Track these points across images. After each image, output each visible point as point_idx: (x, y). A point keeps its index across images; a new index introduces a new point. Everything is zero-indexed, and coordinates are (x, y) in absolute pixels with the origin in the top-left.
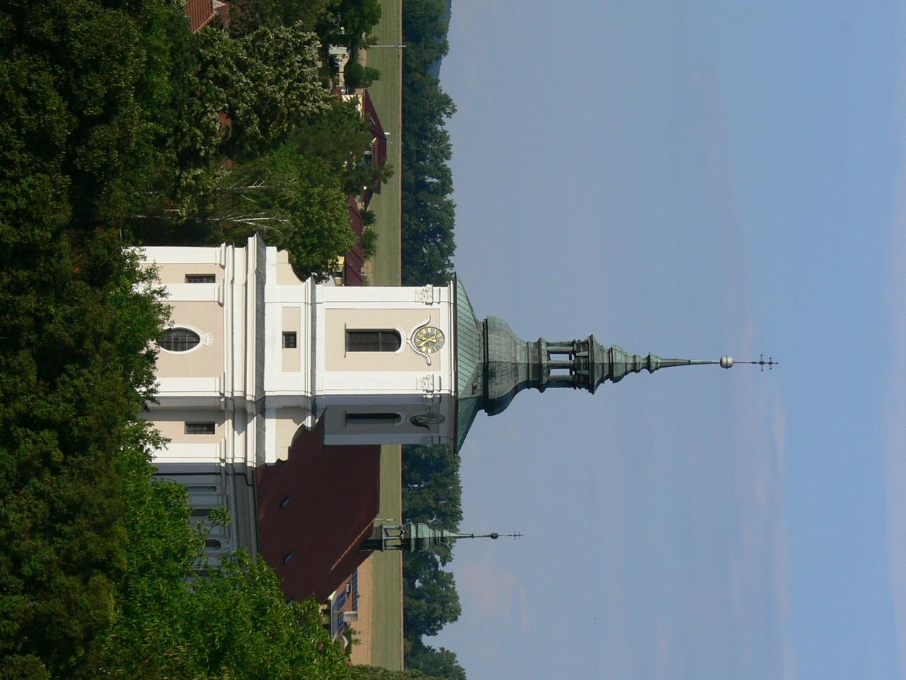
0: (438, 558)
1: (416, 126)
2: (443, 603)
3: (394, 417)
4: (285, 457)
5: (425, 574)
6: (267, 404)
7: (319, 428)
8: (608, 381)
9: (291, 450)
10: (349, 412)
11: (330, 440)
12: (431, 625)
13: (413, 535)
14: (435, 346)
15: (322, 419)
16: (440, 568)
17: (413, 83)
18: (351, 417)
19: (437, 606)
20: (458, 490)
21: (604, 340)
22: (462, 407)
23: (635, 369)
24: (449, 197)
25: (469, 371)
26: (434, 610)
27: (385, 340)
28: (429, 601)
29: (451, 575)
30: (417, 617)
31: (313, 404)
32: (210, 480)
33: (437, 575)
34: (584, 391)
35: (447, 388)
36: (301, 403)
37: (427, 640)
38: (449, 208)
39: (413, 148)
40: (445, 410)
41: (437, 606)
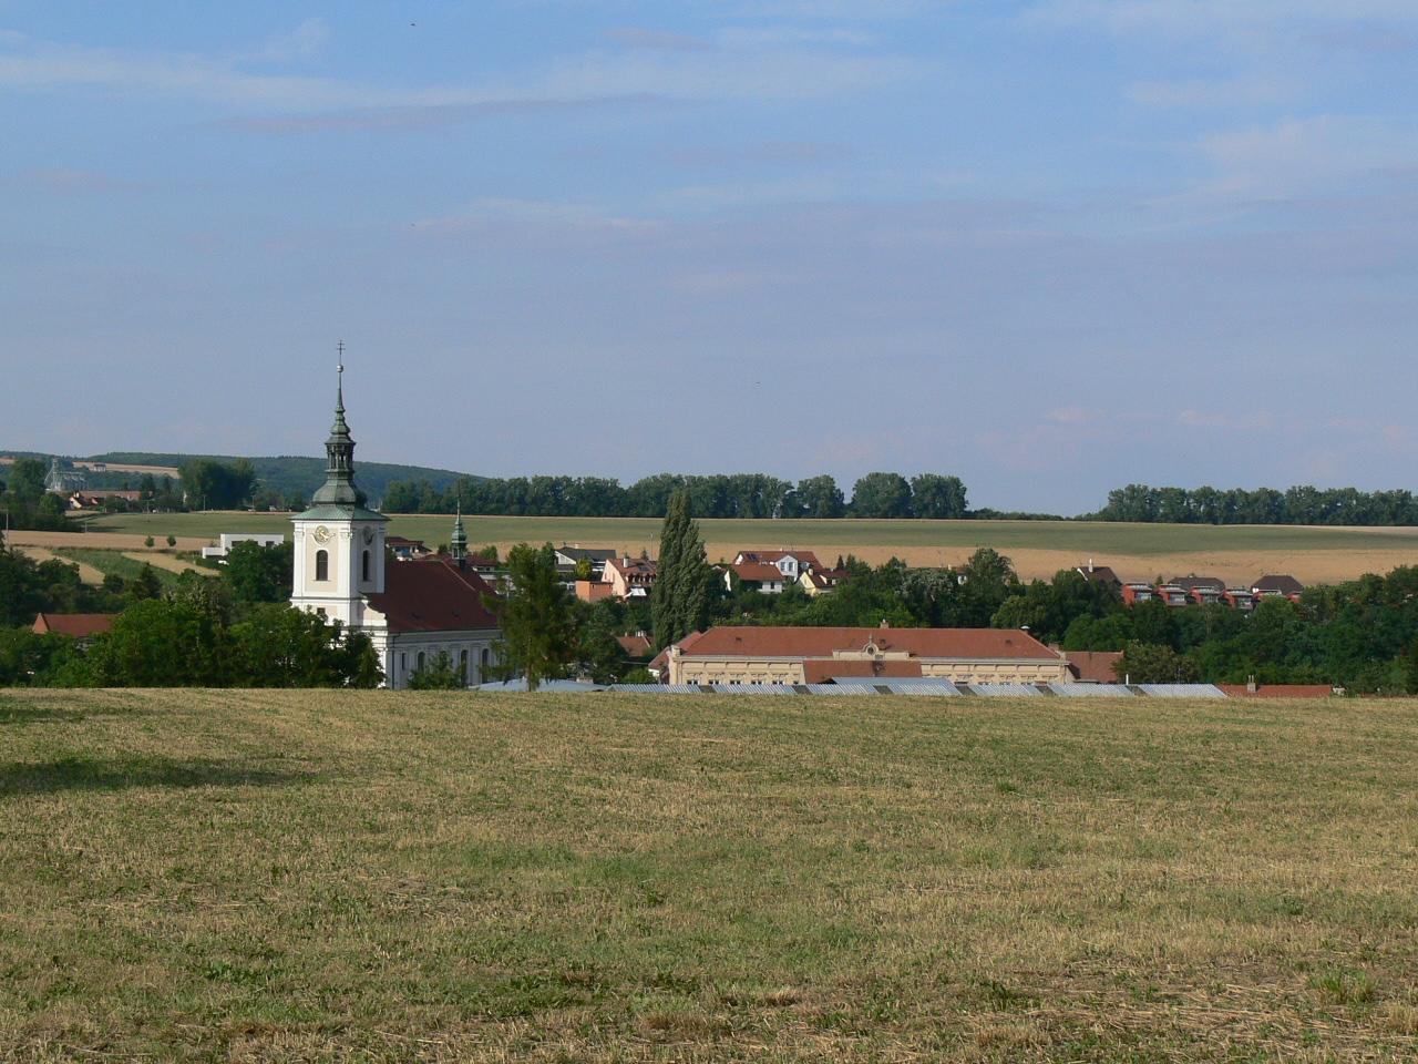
0: (788, 492)
1: (478, 503)
2: (820, 488)
3: (366, 555)
4: (384, 615)
5: (799, 501)
6: (355, 624)
7: (370, 596)
8: (350, 435)
9: (380, 612)
10: (361, 577)
11: (380, 589)
12: (836, 497)
13: (457, 542)
14: (326, 531)
15: (365, 594)
16: (795, 490)
17: (447, 505)
18: (365, 576)
19: (822, 493)
20: (742, 477)
21: (327, 437)
22: (358, 516)
23: (343, 420)
24: (529, 481)
25: (338, 513)
26: (825, 495)
27: (322, 558)
28: (819, 498)
29: (801, 482)
30: (829, 507)
31: (355, 599)
32: (398, 657)
33: (800, 493)
34: (355, 448)
35: (346, 525)
36: (355, 607)
37: (847, 501)
38: (538, 481)
39: (493, 506)
40: (361, 527)
41: (822, 493)
